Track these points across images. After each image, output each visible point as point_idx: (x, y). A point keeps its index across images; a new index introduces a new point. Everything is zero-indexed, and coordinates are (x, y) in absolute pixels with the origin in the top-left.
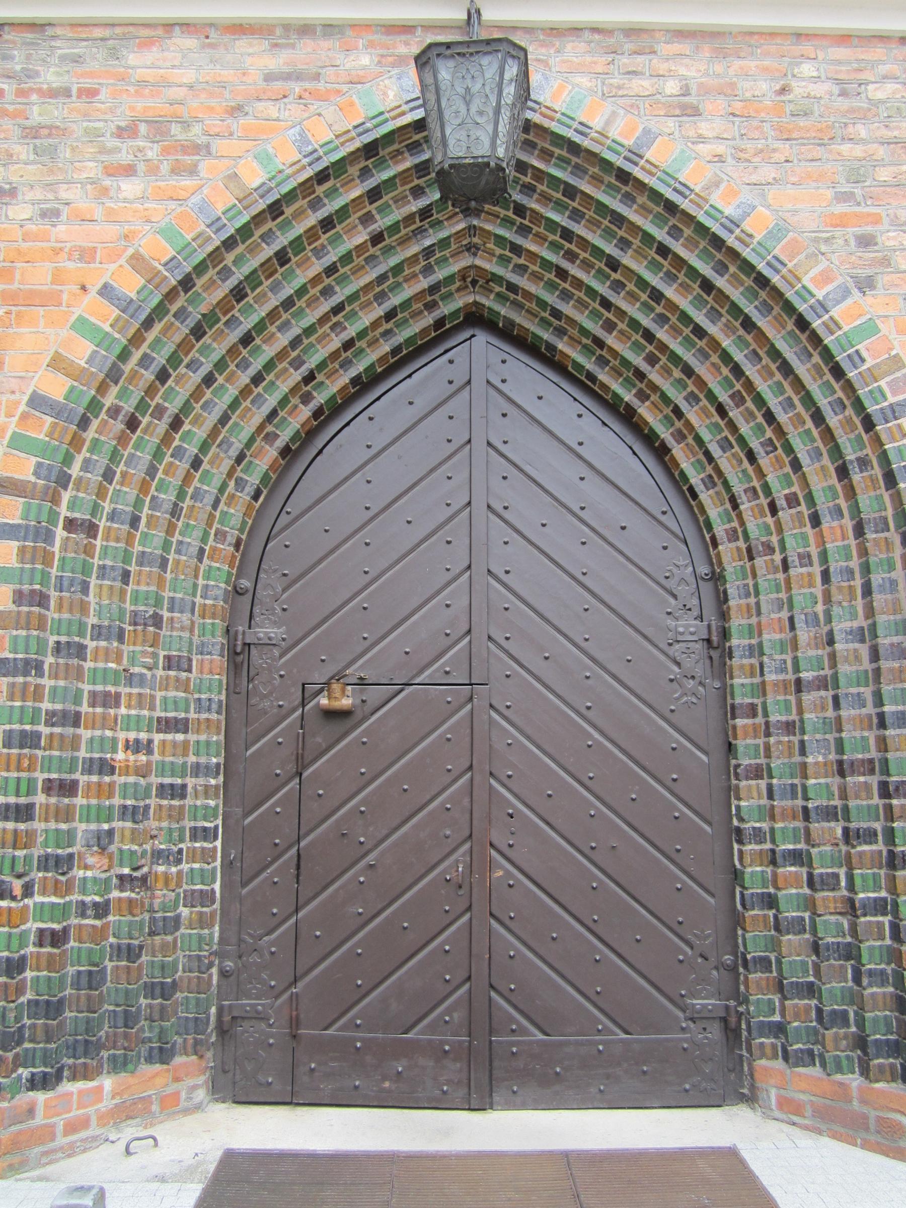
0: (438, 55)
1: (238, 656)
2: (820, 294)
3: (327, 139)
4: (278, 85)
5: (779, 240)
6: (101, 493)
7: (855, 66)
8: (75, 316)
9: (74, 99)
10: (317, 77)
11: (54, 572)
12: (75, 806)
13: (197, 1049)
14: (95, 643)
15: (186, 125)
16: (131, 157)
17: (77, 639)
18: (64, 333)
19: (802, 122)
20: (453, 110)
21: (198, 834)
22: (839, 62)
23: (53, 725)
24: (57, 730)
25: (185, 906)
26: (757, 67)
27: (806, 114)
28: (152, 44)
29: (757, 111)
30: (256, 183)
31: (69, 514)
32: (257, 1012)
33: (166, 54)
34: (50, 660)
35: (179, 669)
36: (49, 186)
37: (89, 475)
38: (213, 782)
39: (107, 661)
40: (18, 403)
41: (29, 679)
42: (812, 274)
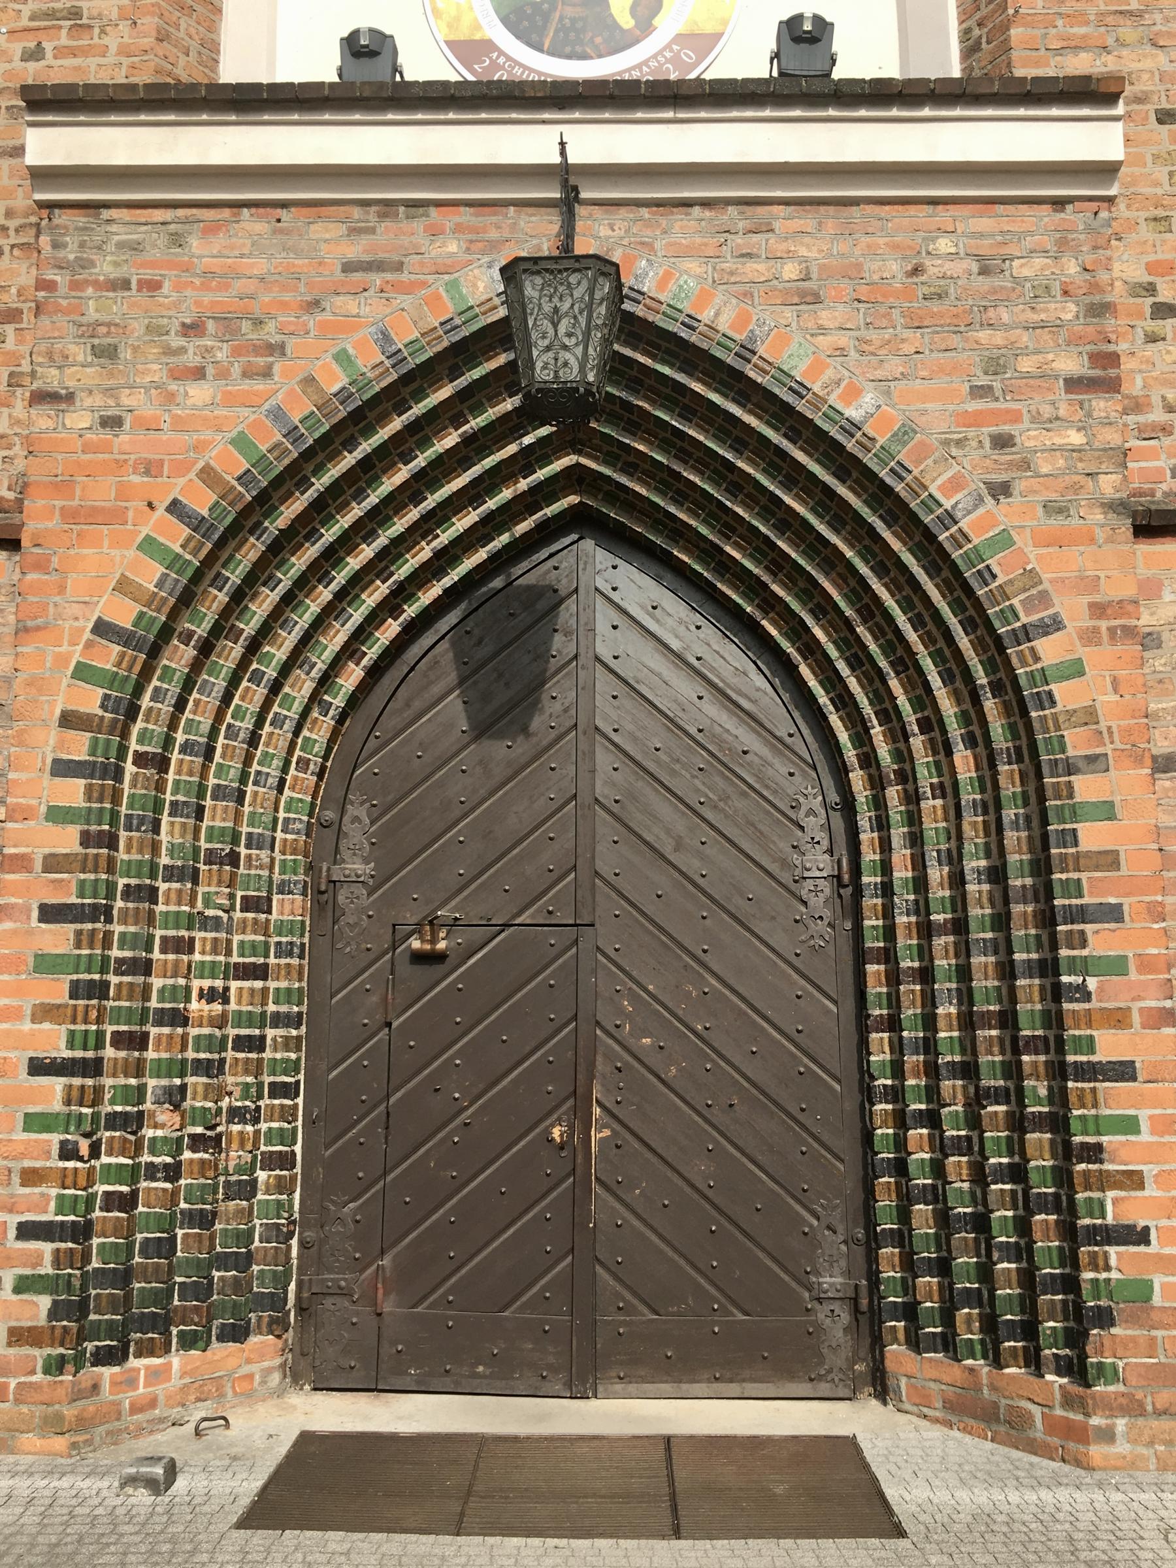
0: (525, 271)
1: (323, 896)
2: (948, 504)
3: (412, 337)
4: (357, 276)
5: (905, 444)
6: (173, 725)
7: (999, 238)
8: (143, 535)
9: (134, 292)
10: (399, 267)
11: (123, 810)
12: (145, 1060)
13: (278, 1326)
14: (167, 885)
15: (258, 323)
16: (198, 359)
17: (148, 881)
18: (131, 553)
19: (935, 306)
20: (540, 330)
21: (278, 1090)
22: (982, 235)
23: (122, 974)
24: (127, 979)
25: (262, 1169)
26: (886, 244)
27: (940, 297)
28: (219, 228)
29: (884, 296)
30: (335, 388)
31: (138, 748)
32: (340, 1288)
33: (234, 240)
34: (119, 904)
35: (258, 911)
36: (109, 391)
37: (159, 705)
38: (294, 1033)
39: (179, 904)
40: (83, 629)
41: (99, 925)
42: (939, 482)
